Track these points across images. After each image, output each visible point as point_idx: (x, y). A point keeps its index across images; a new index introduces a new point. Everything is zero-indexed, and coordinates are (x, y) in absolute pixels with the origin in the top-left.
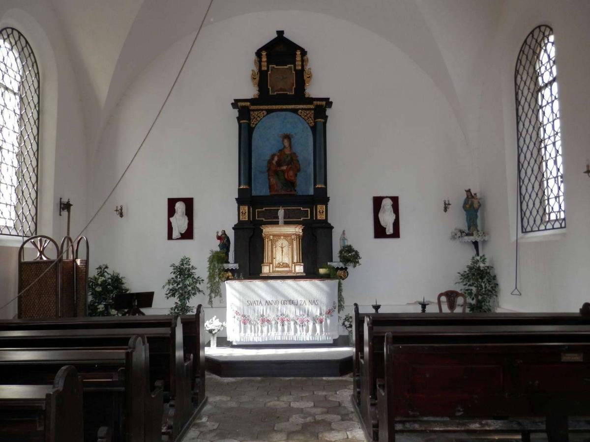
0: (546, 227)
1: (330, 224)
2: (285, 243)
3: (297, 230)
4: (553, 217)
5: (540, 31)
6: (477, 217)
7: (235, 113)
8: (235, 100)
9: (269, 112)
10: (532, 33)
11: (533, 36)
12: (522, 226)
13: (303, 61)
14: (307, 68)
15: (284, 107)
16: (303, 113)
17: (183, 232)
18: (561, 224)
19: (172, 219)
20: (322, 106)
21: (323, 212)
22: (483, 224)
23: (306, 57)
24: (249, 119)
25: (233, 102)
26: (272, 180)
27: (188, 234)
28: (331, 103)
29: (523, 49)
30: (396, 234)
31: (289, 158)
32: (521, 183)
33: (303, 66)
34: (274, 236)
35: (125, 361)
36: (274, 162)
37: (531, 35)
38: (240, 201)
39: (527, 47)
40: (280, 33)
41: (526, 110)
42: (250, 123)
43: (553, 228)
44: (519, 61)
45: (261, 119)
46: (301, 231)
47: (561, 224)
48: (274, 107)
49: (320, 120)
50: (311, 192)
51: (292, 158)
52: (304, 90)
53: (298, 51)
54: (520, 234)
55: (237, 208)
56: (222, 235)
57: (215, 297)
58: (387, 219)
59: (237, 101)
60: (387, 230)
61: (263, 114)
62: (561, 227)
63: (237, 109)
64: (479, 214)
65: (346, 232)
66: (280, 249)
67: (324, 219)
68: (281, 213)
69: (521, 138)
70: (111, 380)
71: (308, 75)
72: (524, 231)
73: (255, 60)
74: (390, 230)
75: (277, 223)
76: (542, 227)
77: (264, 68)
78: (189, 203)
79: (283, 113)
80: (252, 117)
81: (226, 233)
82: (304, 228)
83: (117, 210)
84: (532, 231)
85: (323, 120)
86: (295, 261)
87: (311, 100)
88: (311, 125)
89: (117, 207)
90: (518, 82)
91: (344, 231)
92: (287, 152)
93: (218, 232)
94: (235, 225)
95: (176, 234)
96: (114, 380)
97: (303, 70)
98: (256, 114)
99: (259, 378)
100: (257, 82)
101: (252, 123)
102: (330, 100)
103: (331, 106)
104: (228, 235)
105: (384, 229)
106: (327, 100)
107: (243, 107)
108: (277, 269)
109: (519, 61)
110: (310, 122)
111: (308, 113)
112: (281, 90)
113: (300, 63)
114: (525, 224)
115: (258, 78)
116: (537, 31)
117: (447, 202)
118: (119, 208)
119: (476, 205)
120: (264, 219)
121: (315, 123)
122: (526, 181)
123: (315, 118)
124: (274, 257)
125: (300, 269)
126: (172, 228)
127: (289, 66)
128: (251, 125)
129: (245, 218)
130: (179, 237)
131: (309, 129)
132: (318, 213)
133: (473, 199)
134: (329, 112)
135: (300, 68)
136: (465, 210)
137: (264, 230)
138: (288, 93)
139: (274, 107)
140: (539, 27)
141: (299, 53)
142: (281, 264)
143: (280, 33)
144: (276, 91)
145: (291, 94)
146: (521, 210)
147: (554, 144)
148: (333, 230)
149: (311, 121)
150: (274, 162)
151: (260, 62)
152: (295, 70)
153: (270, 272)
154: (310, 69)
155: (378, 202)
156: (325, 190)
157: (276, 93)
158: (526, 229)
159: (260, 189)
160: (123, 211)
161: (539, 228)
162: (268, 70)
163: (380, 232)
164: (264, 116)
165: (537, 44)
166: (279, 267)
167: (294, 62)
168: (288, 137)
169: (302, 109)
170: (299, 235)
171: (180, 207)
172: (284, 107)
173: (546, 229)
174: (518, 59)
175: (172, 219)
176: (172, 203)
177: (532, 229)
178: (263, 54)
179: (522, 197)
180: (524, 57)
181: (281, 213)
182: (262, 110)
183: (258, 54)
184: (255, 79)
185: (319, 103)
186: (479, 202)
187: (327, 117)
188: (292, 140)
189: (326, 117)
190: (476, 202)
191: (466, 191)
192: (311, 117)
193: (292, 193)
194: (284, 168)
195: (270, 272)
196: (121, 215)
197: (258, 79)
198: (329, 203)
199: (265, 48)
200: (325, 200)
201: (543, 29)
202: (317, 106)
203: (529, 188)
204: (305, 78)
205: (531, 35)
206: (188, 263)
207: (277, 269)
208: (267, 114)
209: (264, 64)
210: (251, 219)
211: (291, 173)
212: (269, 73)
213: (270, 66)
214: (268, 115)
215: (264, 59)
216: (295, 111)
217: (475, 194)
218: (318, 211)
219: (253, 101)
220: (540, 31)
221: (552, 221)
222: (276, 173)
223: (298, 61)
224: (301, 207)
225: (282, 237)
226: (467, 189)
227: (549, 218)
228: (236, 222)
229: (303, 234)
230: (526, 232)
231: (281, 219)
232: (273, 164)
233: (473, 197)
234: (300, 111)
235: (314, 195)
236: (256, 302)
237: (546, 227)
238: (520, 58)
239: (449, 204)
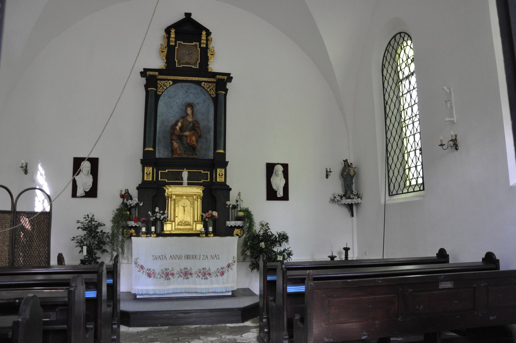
0: (408, 190)
1: (229, 186)
2: (187, 203)
3: (198, 191)
4: (414, 182)
5: (401, 36)
6: (352, 183)
7: (143, 81)
8: (144, 69)
9: (175, 82)
10: (394, 37)
11: (395, 40)
12: (389, 190)
13: (207, 40)
14: (211, 46)
15: (189, 78)
16: (206, 85)
17: (87, 190)
18: (420, 188)
19: (77, 178)
20: (224, 80)
21: (223, 175)
22: (357, 189)
23: (209, 37)
24: (156, 88)
25: (143, 71)
26: (175, 144)
27: (92, 193)
28: (232, 78)
29: (388, 49)
30: (285, 197)
31: (191, 125)
32: (388, 155)
33: (207, 44)
34: (177, 195)
35: (67, 299)
36: (178, 128)
37: (394, 39)
38: (145, 162)
39: (391, 48)
40: (188, 15)
41: (391, 96)
42: (157, 91)
43: (414, 191)
44: (385, 58)
45: (167, 88)
46: (202, 192)
47: (420, 188)
48: (180, 78)
49: (221, 92)
50: (211, 156)
51: (194, 125)
52: (208, 65)
53: (204, 31)
54: (388, 197)
55: (26, 189)
56: (125, 194)
57: (230, 204)
58: (278, 182)
59: (146, 70)
60: (278, 193)
61: (169, 83)
62: (420, 190)
63: (145, 77)
64: (354, 180)
65: (241, 194)
66: (183, 208)
67: (223, 181)
68: (185, 174)
69: (388, 118)
70: (49, 320)
71: (212, 52)
72: (391, 194)
73: (164, 36)
74: (280, 194)
75: (181, 184)
76: (405, 191)
77: (172, 44)
78: (94, 162)
79: (188, 84)
80: (159, 86)
81: (129, 192)
82: (204, 189)
83: (22, 167)
84: (397, 194)
85: (223, 92)
86: (196, 220)
87: (214, 75)
88: (213, 96)
89: (22, 164)
90: (385, 74)
91: (239, 193)
92: (190, 119)
93: (121, 191)
94: (139, 185)
95: (80, 192)
96: (52, 319)
97: (207, 48)
98: (163, 83)
99: (167, 327)
100: (165, 55)
101: (159, 90)
102: (231, 76)
103: (231, 80)
104: (131, 194)
105: (275, 192)
106: (228, 75)
107: (150, 76)
108: (179, 227)
109: (385, 58)
110: (212, 93)
111: (210, 85)
112: (187, 63)
113: (205, 42)
114: (392, 188)
115: (166, 51)
116: (399, 35)
117: (328, 170)
118: (24, 165)
119: (352, 173)
120: (202, 172)
121: (217, 94)
122: (392, 153)
123: (217, 90)
124: (176, 215)
125: (200, 227)
126: (77, 186)
127: (195, 43)
128: (158, 92)
129: (149, 179)
130: (83, 195)
131: (211, 100)
132: (218, 176)
133: (349, 168)
134: (229, 86)
135: (204, 46)
136: (343, 178)
137: (167, 191)
138: (193, 67)
139: (180, 78)
140: (400, 33)
141: (205, 33)
142: (183, 222)
143: (188, 15)
144: (183, 64)
145: (195, 67)
146: (389, 176)
147: (416, 167)
148: (231, 192)
149: (213, 93)
150: (178, 128)
151: (169, 38)
152: (200, 47)
153: (172, 230)
154: (213, 47)
155: (270, 168)
156: (224, 155)
157: (182, 66)
158: (392, 193)
159: (161, 153)
160: (28, 168)
161: (402, 192)
162: (175, 45)
163: (271, 195)
164: (170, 86)
165: (398, 46)
166: (181, 225)
167: (199, 40)
168: (191, 105)
169: (205, 82)
170: (200, 195)
171: (86, 166)
172: (189, 78)
173: (408, 192)
174: (384, 56)
175: (77, 178)
176: (77, 162)
177: (397, 192)
178: (172, 31)
179: (389, 166)
180: (389, 54)
181: (185, 174)
182: (169, 80)
183: (168, 31)
184: (163, 52)
185: (221, 77)
186: (354, 171)
187: (227, 90)
188: (194, 108)
189: (226, 90)
190: (352, 170)
191: (343, 160)
192: (212, 89)
193: (194, 157)
194: (187, 133)
195: (172, 230)
196: (26, 172)
197: (166, 52)
198: (227, 167)
199: (174, 26)
200: (224, 164)
201: (403, 35)
202: (219, 80)
203: (394, 159)
204: (209, 55)
205: (394, 39)
206: (92, 220)
207: (179, 227)
208: (173, 84)
209: (172, 39)
210: (155, 180)
211: (194, 138)
212: (177, 48)
213: (178, 42)
214: (174, 85)
215: (173, 35)
216: (199, 83)
217: (351, 164)
218: (218, 173)
219: (160, 71)
220: (401, 36)
221: (413, 185)
222: (180, 138)
223: (203, 40)
224: (202, 170)
225: (184, 197)
226: (345, 159)
227: (410, 183)
228: (140, 182)
229: (203, 195)
230: (392, 195)
231: (185, 181)
232: (176, 129)
233: (349, 166)
234: (203, 83)
235: (213, 160)
236: (161, 257)
237: (408, 190)
238: (386, 55)
239: (330, 172)
